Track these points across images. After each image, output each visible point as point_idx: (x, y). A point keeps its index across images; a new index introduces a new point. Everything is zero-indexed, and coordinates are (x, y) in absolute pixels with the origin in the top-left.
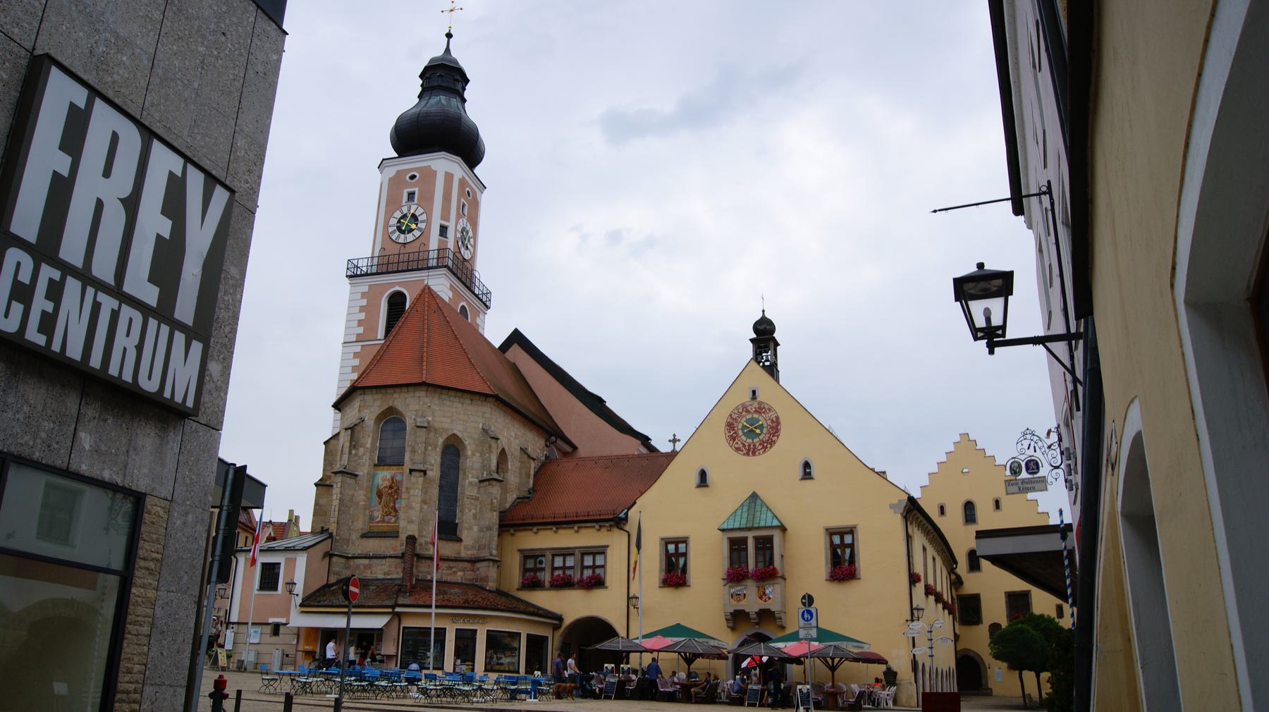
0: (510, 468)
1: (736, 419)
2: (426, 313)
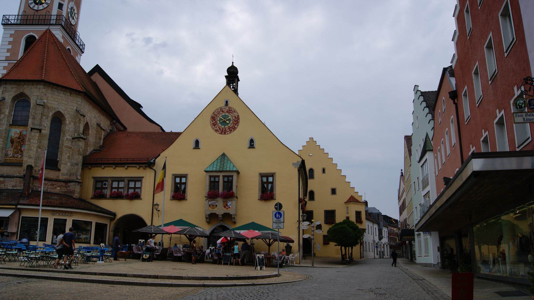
0: (90, 133)
1: (216, 115)
2: (47, 43)
